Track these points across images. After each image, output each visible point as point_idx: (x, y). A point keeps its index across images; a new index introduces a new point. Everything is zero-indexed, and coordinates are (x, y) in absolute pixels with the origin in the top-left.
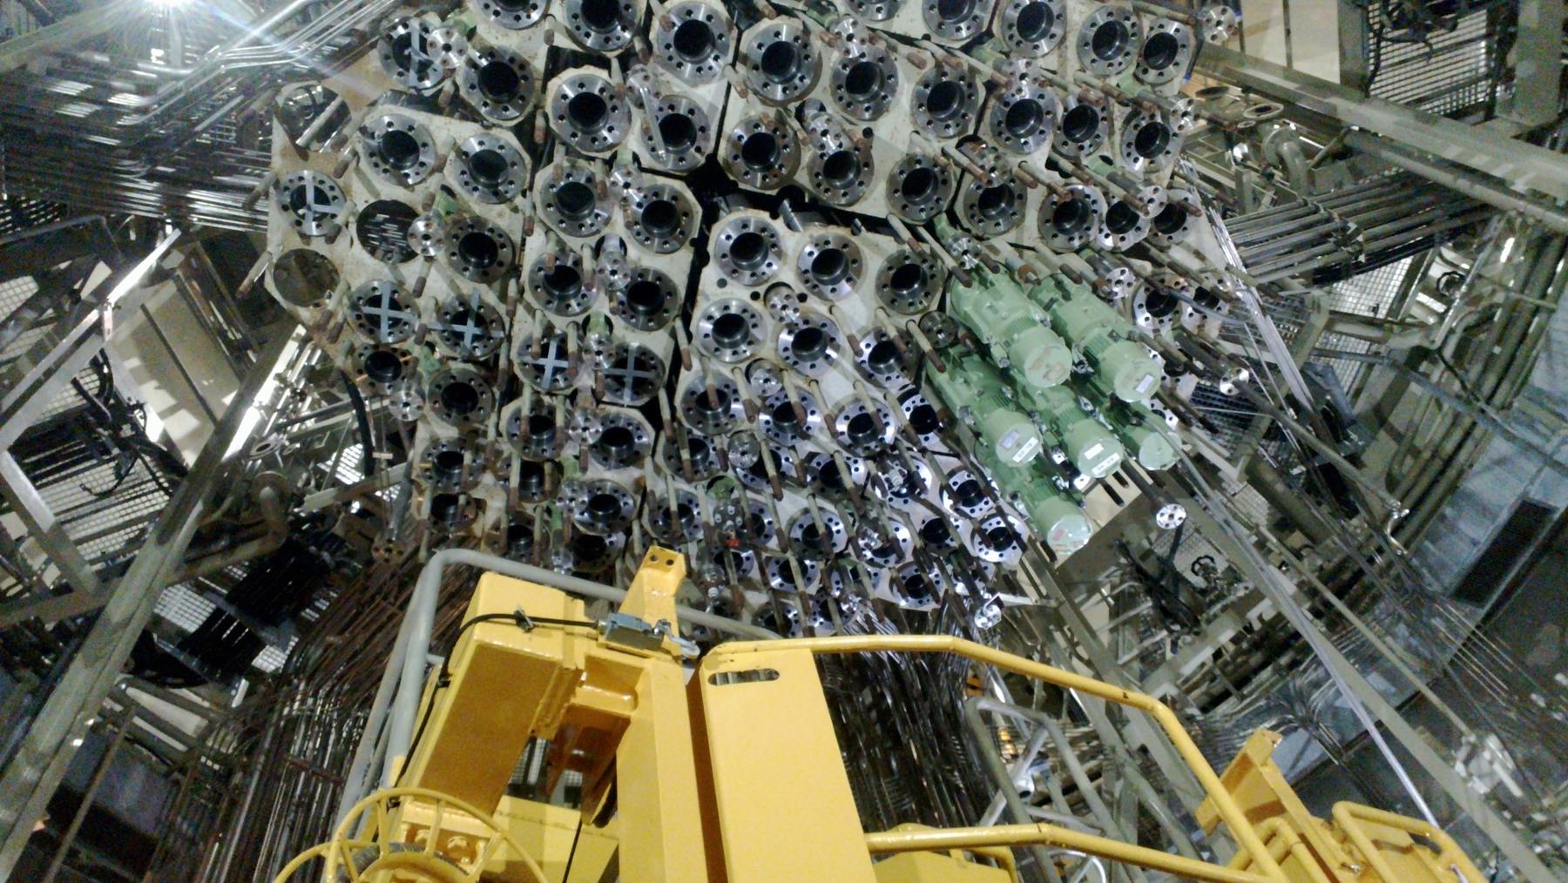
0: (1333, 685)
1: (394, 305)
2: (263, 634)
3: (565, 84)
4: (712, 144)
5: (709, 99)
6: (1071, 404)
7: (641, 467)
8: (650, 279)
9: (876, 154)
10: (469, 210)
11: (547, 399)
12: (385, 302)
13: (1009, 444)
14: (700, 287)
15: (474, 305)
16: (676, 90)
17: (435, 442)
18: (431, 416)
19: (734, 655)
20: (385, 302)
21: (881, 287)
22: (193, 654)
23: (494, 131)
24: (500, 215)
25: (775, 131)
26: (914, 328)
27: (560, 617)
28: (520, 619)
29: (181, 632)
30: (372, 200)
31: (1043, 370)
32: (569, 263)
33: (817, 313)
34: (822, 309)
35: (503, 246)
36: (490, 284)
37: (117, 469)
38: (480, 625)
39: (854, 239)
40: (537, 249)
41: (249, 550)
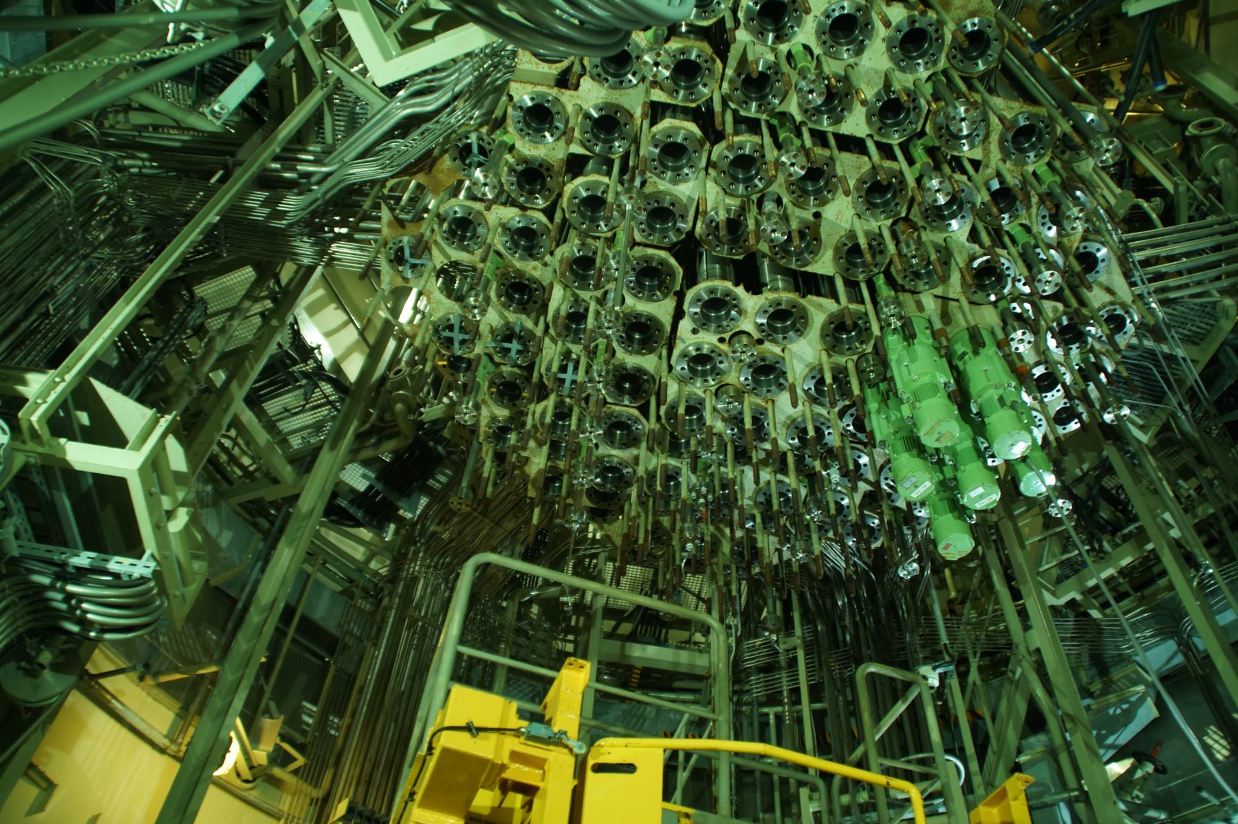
0: (1224, 598)
1: (462, 329)
2: (400, 504)
3: (576, 187)
4: (691, 224)
5: (688, 193)
6: (968, 443)
7: (639, 448)
8: (643, 320)
9: (823, 232)
10: (513, 266)
11: (568, 400)
12: (456, 328)
13: (907, 484)
15: (517, 330)
16: (661, 188)
17: (494, 418)
18: (490, 402)
19: (613, 749)
20: (456, 328)
21: (824, 335)
22: (359, 507)
23: (529, 213)
24: (534, 268)
25: (739, 216)
26: (851, 366)
27: (497, 726)
28: (469, 728)
29: (353, 490)
30: (446, 261)
31: (936, 436)
32: (582, 310)
33: (772, 352)
34: (777, 350)
35: (536, 290)
36: (528, 315)
37: (305, 394)
38: (445, 733)
39: (802, 301)
40: (558, 299)
41: (391, 445)
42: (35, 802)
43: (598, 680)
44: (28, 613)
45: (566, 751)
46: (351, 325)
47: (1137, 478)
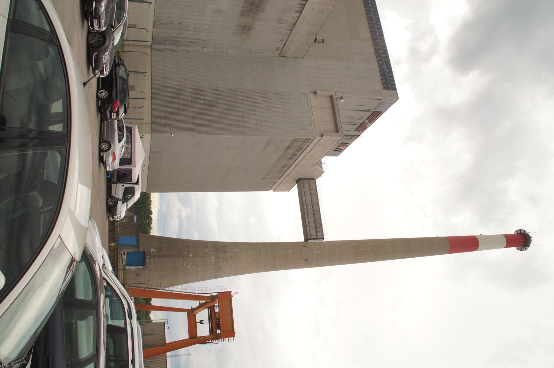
14: (90, 191)
43: (382, 77)
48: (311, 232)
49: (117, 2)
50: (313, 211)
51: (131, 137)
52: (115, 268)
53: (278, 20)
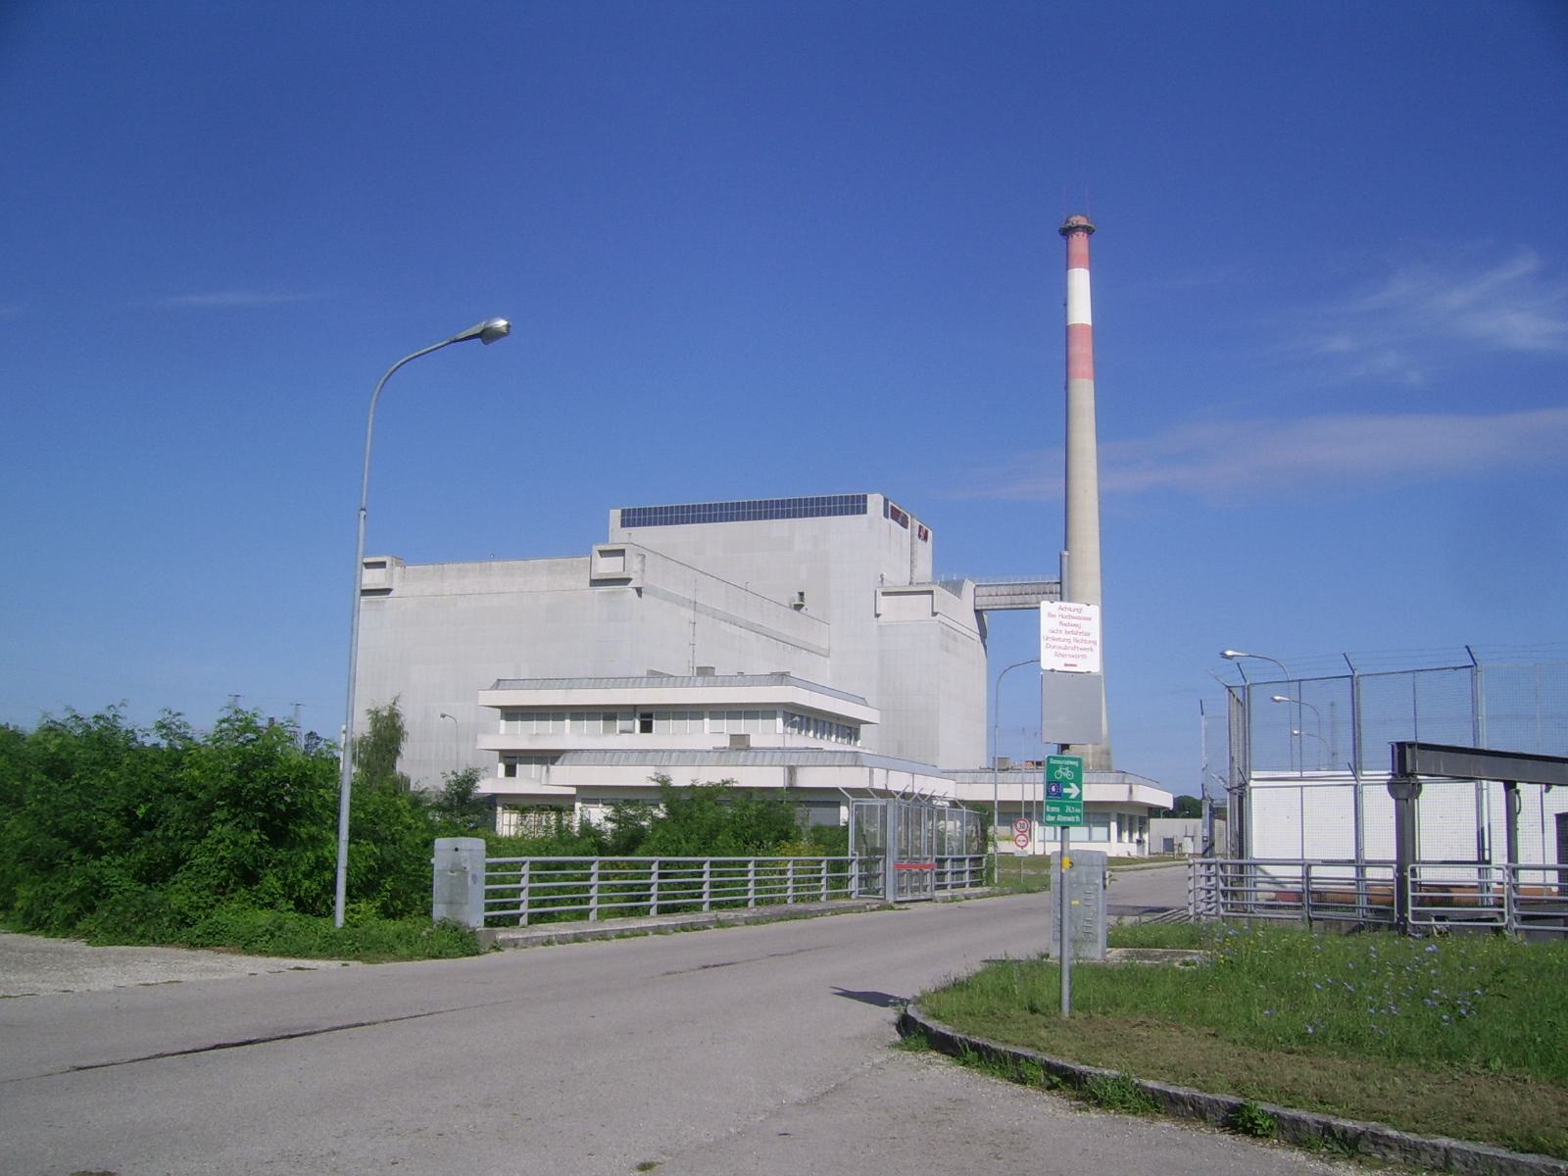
14: (1092, 383)
42: (1516, 839)
43: (316, 905)
44: (352, 740)
45: (972, 767)
46: (1304, 788)
47: (766, 884)
48: (985, 603)
49: (591, 930)
50: (1021, 594)
51: (860, 819)
52: (1328, 1129)
53: (161, 726)
